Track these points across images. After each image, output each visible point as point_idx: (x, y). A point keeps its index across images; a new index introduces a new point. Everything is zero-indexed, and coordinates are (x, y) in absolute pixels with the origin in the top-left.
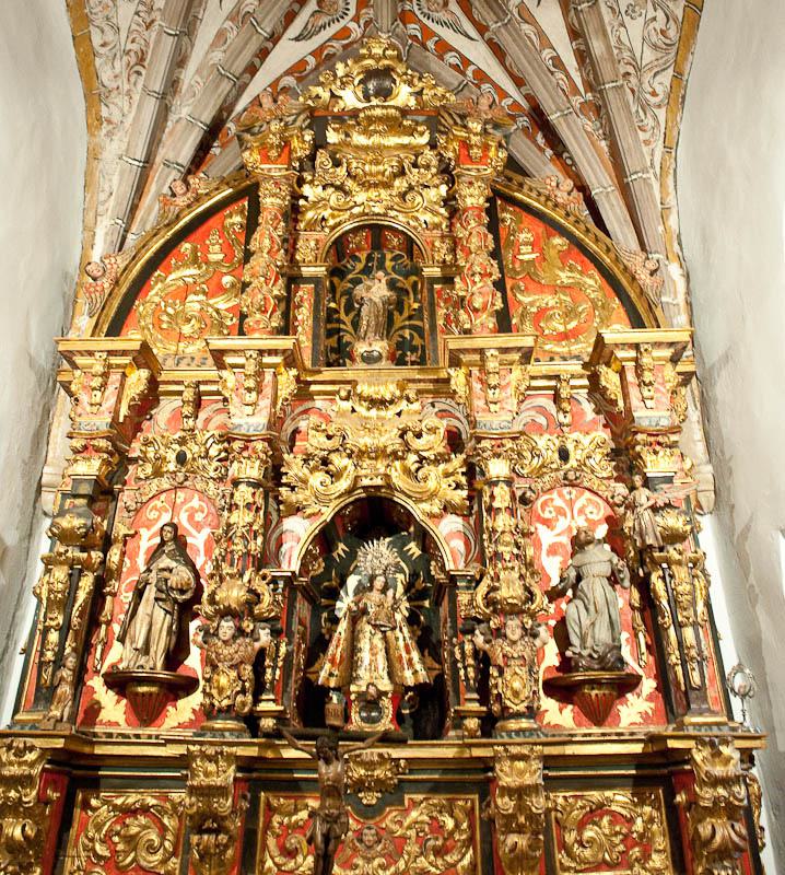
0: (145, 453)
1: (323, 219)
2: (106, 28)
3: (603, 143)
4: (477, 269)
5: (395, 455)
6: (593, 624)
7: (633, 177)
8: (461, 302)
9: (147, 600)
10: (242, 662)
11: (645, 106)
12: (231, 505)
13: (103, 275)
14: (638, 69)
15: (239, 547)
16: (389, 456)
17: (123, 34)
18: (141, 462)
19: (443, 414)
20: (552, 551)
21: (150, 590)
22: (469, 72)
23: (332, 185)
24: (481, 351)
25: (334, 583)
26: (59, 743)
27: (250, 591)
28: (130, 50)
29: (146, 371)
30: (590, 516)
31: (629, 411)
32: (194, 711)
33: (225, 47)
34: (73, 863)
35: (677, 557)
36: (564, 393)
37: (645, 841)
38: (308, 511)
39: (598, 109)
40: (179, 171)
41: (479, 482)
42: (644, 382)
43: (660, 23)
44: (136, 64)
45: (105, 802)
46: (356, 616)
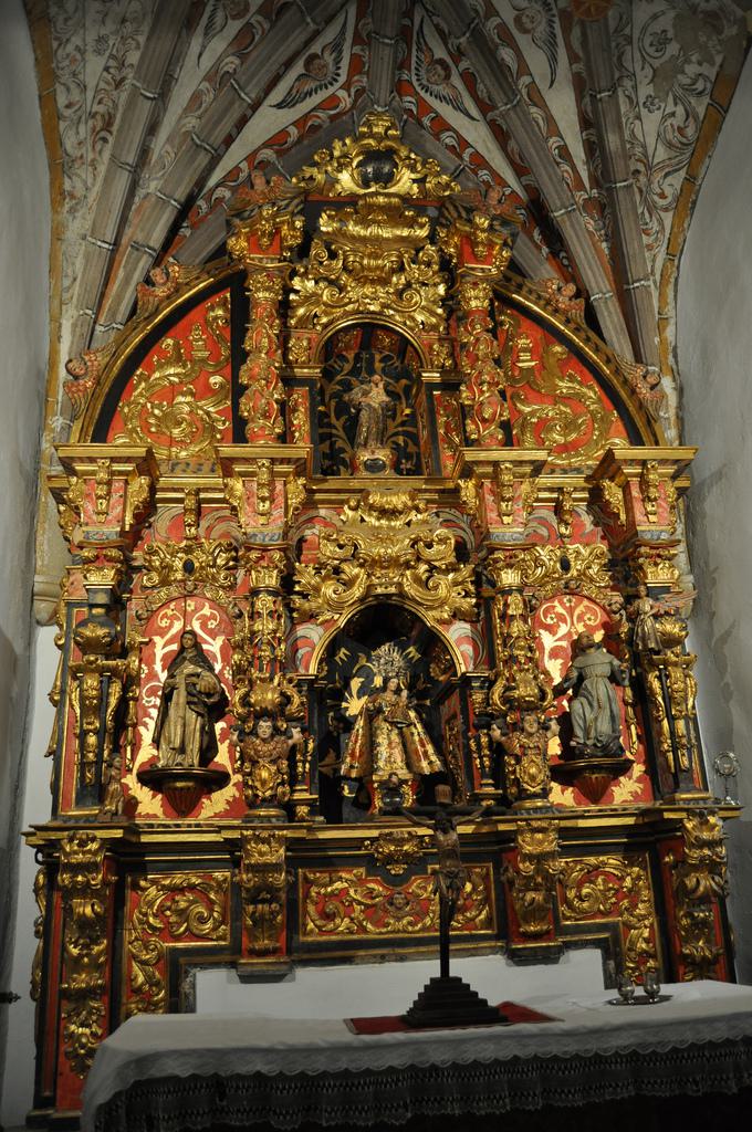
0: (150, 561)
1: (315, 315)
2: (72, 86)
3: (604, 245)
4: (486, 377)
5: (407, 565)
6: (596, 719)
7: (636, 285)
8: (464, 412)
9: (177, 704)
10: (279, 758)
11: (652, 208)
12: (253, 613)
13: (86, 374)
14: (649, 167)
15: (266, 653)
16: (401, 565)
17: (90, 94)
18: (145, 571)
19: (447, 523)
20: (555, 654)
21: (178, 695)
22: (466, 156)
23: (326, 279)
24: (496, 464)
25: (338, 684)
26: (118, 834)
27: (283, 694)
28: (96, 113)
29: (147, 478)
30: (588, 622)
31: (632, 523)
32: (228, 802)
33: (199, 112)
34: (131, 934)
35: (675, 659)
36: (567, 506)
37: (633, 894)
38: (321, 619)
39: (602, 208)
40: (150, 254)
41: (487, 591)
42: (649, 498)
43: (678, 121)
44: (102, 130)
45: (154, 882)
46: (372, 715)
